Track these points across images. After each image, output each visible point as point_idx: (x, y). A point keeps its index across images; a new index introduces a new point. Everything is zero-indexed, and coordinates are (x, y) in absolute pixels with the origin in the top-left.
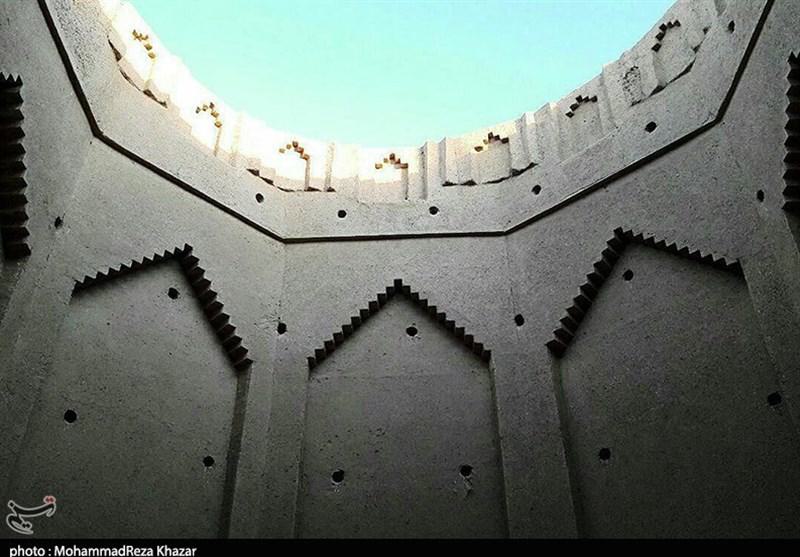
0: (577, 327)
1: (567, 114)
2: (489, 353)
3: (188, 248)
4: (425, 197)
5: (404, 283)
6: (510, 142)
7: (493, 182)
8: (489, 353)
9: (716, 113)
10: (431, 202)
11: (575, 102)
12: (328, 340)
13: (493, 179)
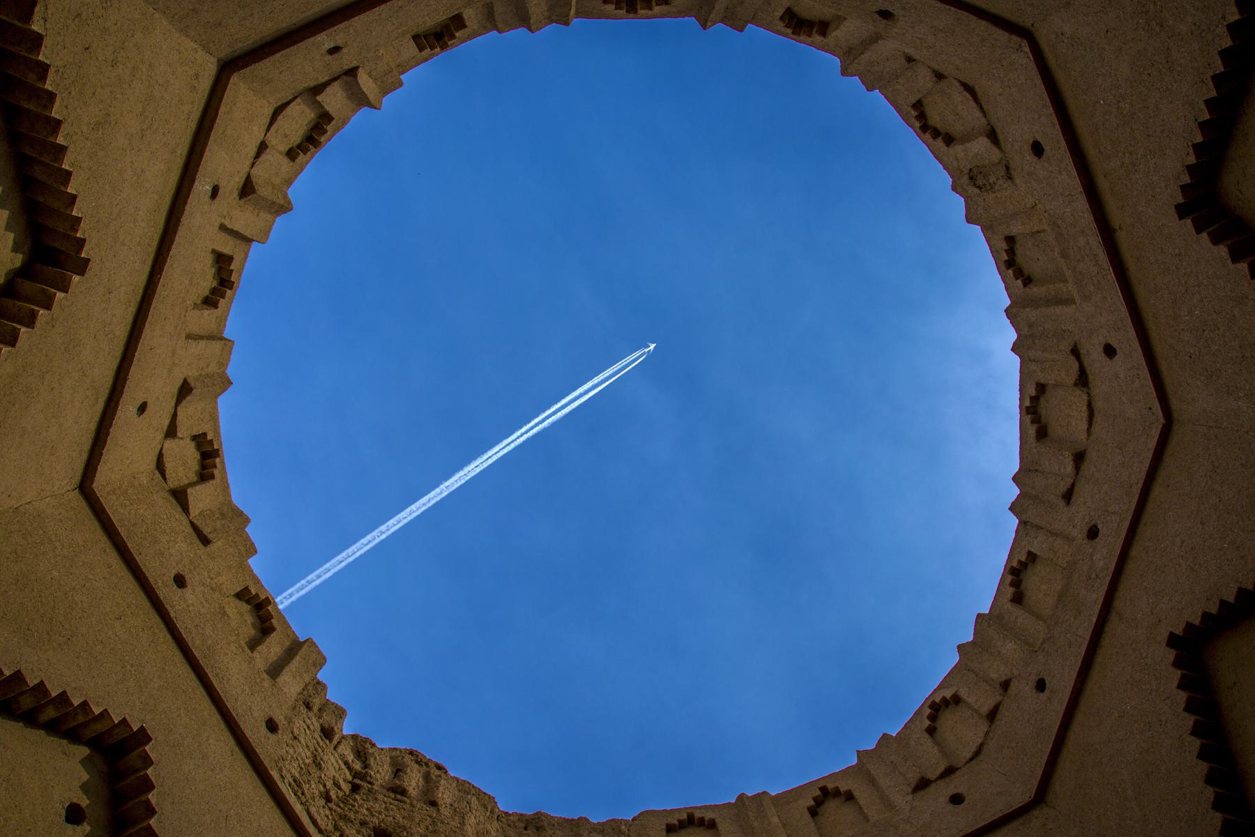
2: (212, 477)
4: (1069, 539)
5: (1179, 631)
9: (1015, 38)
10: (1079, 533)
12: (48, 686)
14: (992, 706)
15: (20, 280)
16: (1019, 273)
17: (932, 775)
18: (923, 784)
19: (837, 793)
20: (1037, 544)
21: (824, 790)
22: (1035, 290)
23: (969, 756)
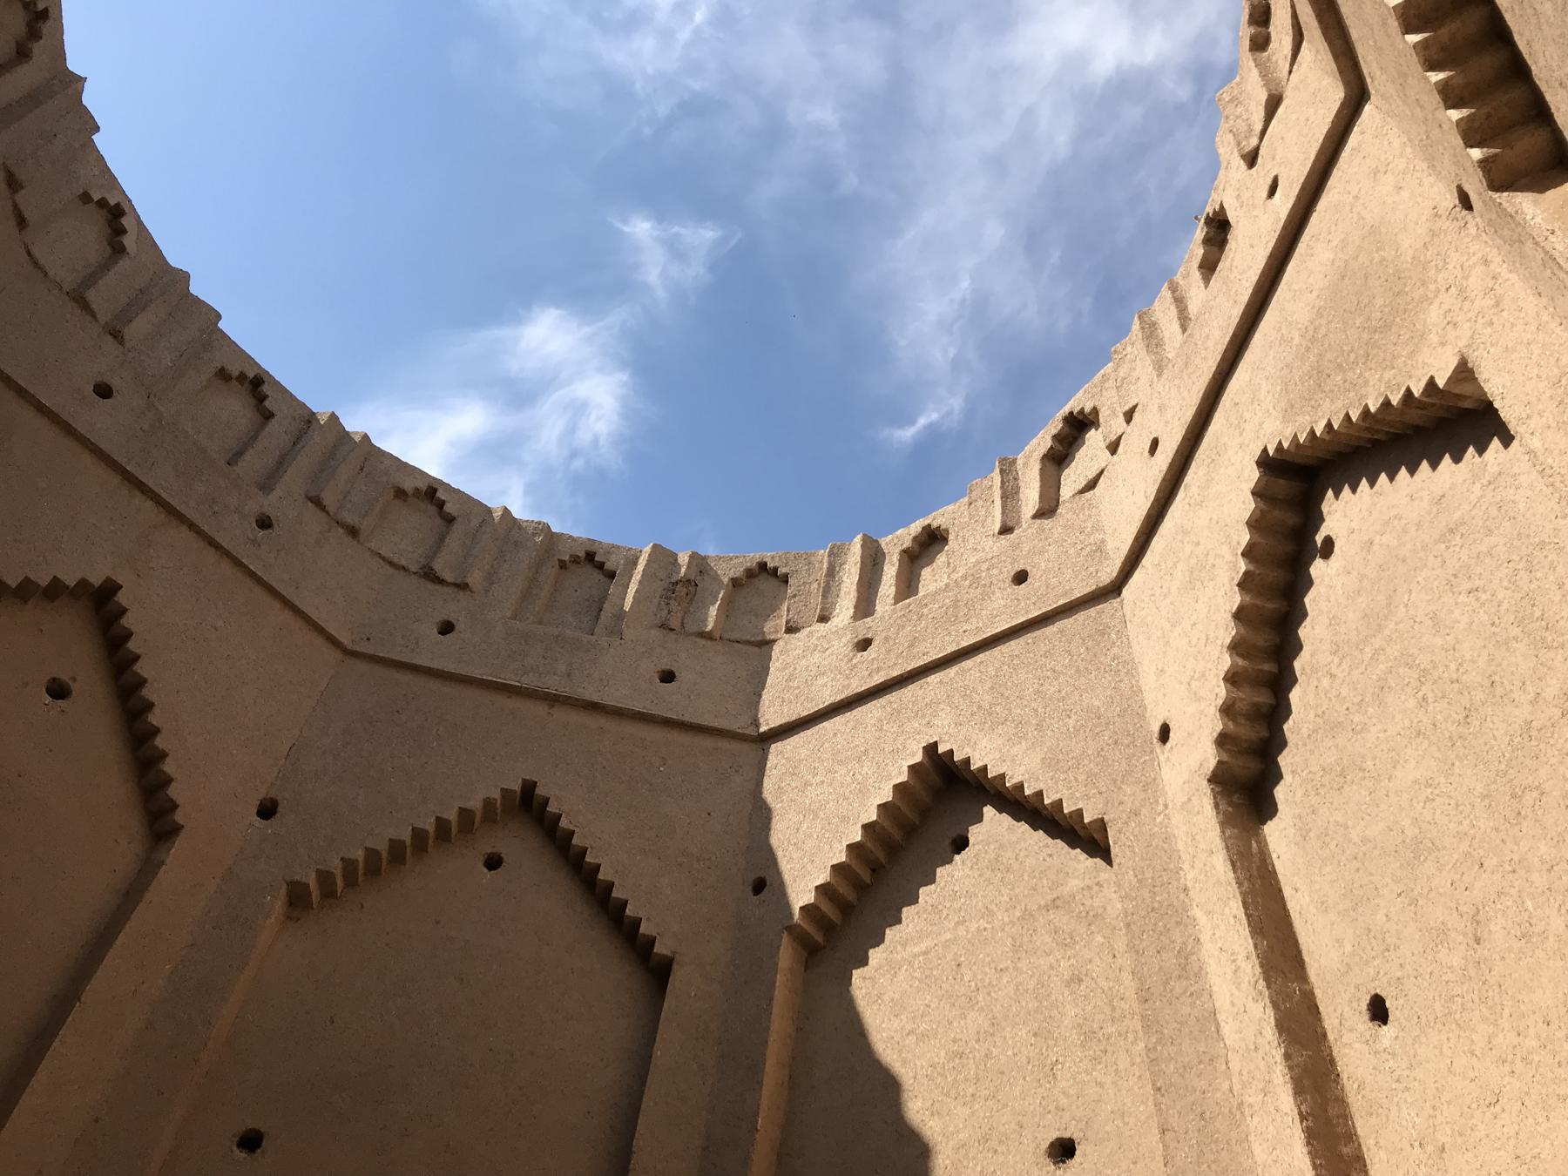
0: (494, 821)
2: (176, 829)
7: (384, 559)
8: (176, 829)
10: (269, 504)
11: (582, 554)
14: (94, 306)
15: (1265, 734)
16: (575, 560)
20: (277, 431)
22: (550, 571)
23: (35, 251)
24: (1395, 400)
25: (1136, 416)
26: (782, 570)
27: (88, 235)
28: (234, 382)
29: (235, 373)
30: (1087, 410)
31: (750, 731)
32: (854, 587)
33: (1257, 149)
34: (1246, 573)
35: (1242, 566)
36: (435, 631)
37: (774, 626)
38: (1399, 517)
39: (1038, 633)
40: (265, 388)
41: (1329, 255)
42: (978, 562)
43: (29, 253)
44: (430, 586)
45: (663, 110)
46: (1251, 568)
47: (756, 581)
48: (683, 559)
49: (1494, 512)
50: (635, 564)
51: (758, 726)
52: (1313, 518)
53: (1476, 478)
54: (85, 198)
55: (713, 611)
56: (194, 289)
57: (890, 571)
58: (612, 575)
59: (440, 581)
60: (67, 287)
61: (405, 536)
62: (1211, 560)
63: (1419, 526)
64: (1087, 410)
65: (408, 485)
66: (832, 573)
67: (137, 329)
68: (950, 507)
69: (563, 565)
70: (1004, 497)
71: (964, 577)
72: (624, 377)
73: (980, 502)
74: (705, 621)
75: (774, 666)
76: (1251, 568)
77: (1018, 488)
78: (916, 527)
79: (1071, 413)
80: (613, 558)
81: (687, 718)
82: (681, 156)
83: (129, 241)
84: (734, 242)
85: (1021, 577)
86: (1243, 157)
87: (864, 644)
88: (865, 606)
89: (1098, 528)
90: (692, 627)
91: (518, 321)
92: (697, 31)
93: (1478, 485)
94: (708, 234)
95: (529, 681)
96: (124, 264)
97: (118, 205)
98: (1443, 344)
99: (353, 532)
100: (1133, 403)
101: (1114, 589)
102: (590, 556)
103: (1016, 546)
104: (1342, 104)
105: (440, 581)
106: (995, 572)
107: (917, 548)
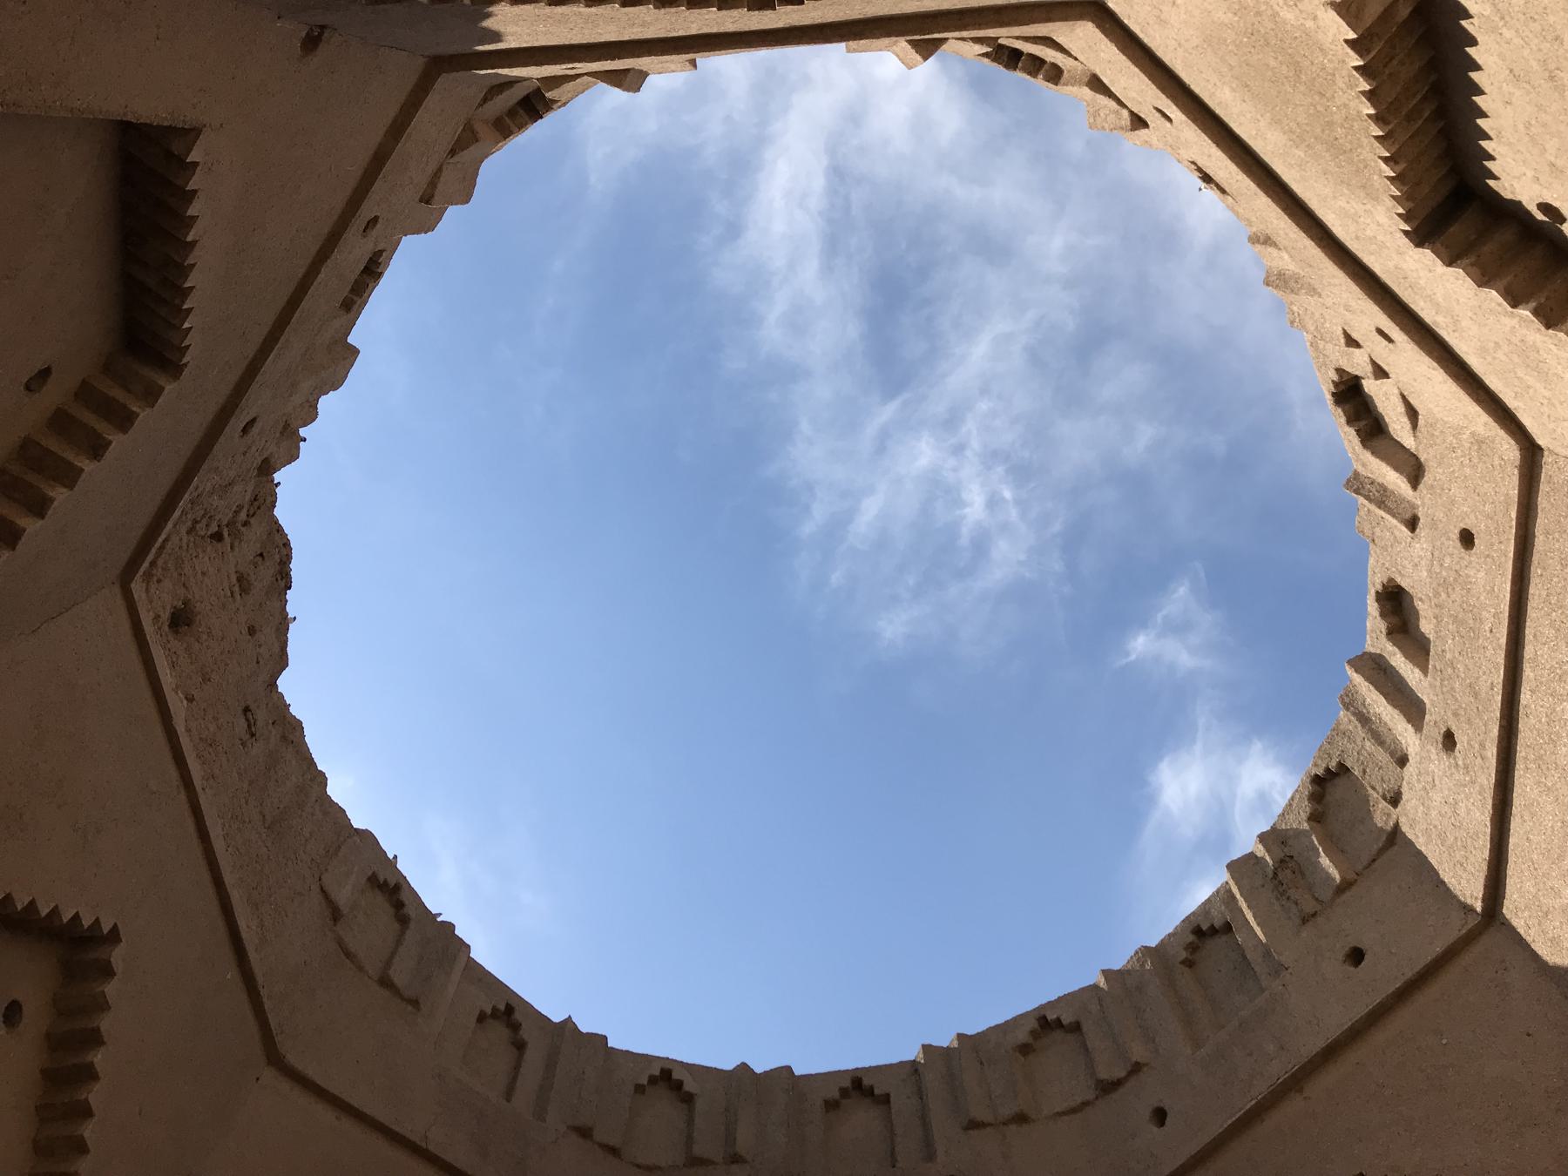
1: (1182, 962)
3: (114, 936)
6: (1085, 1029)
13: (1064, 1106)
16: (1192, 948)
17: (598, 1136)
18: (584, 1132)
19: (515, 1027)
20: (902, 1102)
21: (510, 1010)
24: (1365, 86)
25: (1355, 336)
26: (1333, 765)
27: (663, 1107)
28: (844, 1101)
29: (836, 1095)
30: (1336, 378)
31: (1472, 922)
32: (1390, 708)
33: (1132, 113)
34: (1536, 313)
35: (1525, 313)
36: (1155, 1129)
37: (1382, 815)
38: (1528, 126)
39: (1535, 558)
40: (866, 1082)
41: (1227, 90)
42: (1429, 571)
43: (638, 1166)
44: (1115, 1096)
45: (1058, 566)
46: (1533, 304)
47: (1328, 798)
48: (1260, 851)
49: (1536, 27)
50: (1233, 897)
51: (1471, 909)
52: (1511, 212)
53: (1494, 30)
54: (639, 1089)
55: (1325, 861)
56: (759, 1068)
57: (1398, 661)
58: (1228, 928)
59: (1116, 1084)
60: (1090, 1096)
61: (1060, 1077)
62: (1515, 340)
63: (1540, 107)
64: (1336, 378)
65: (1022, 1036)
66: (1364, 719)
67: (745, 1139)
68: (1371, 561)
69: (1189, 963)
70: (1381, 504)
71: (1437, 594)
72: (1258, 746)
73: (1377, 530)
74: (1329, 877)
75: (1421, 844)
76: (1533, 304)
77: (1381, 485)
78: (1373, 608)
79: (1333, 394)
80: (1214, 913)
81: (1419, 966)
82: (1106, 574)
83: (689, 1086)
84: (1202, 575)
85: (1467, 539)
86: (1134, 128)
87: (1449, 741)
88: (1414, 710)
89: (1457, 432)
90: (1325, 894)
91: (1151, 800)
92: (1018, 502)
93: (1504, 30)
94: (1181, 593)
95: (1261, 1088)
96: (700, 1105)
97: (663, 1070)
98: (1315, 18)
99: (1021, 1118)
100: (1340, 332)
101: (1532, 453)
102: (1198, 932)
103: (1434, 525)
104: (1098, 26)
105: (1116, 1084)
106: (1448, 560)
107: (1395, 620)
